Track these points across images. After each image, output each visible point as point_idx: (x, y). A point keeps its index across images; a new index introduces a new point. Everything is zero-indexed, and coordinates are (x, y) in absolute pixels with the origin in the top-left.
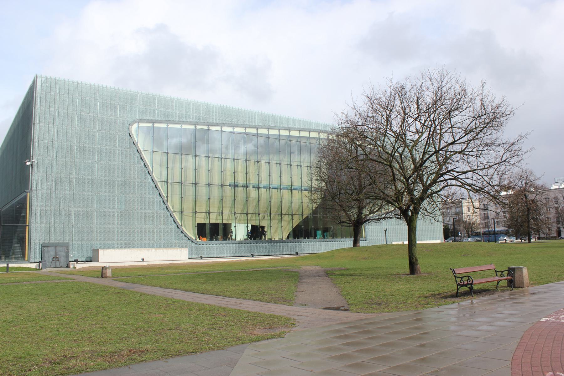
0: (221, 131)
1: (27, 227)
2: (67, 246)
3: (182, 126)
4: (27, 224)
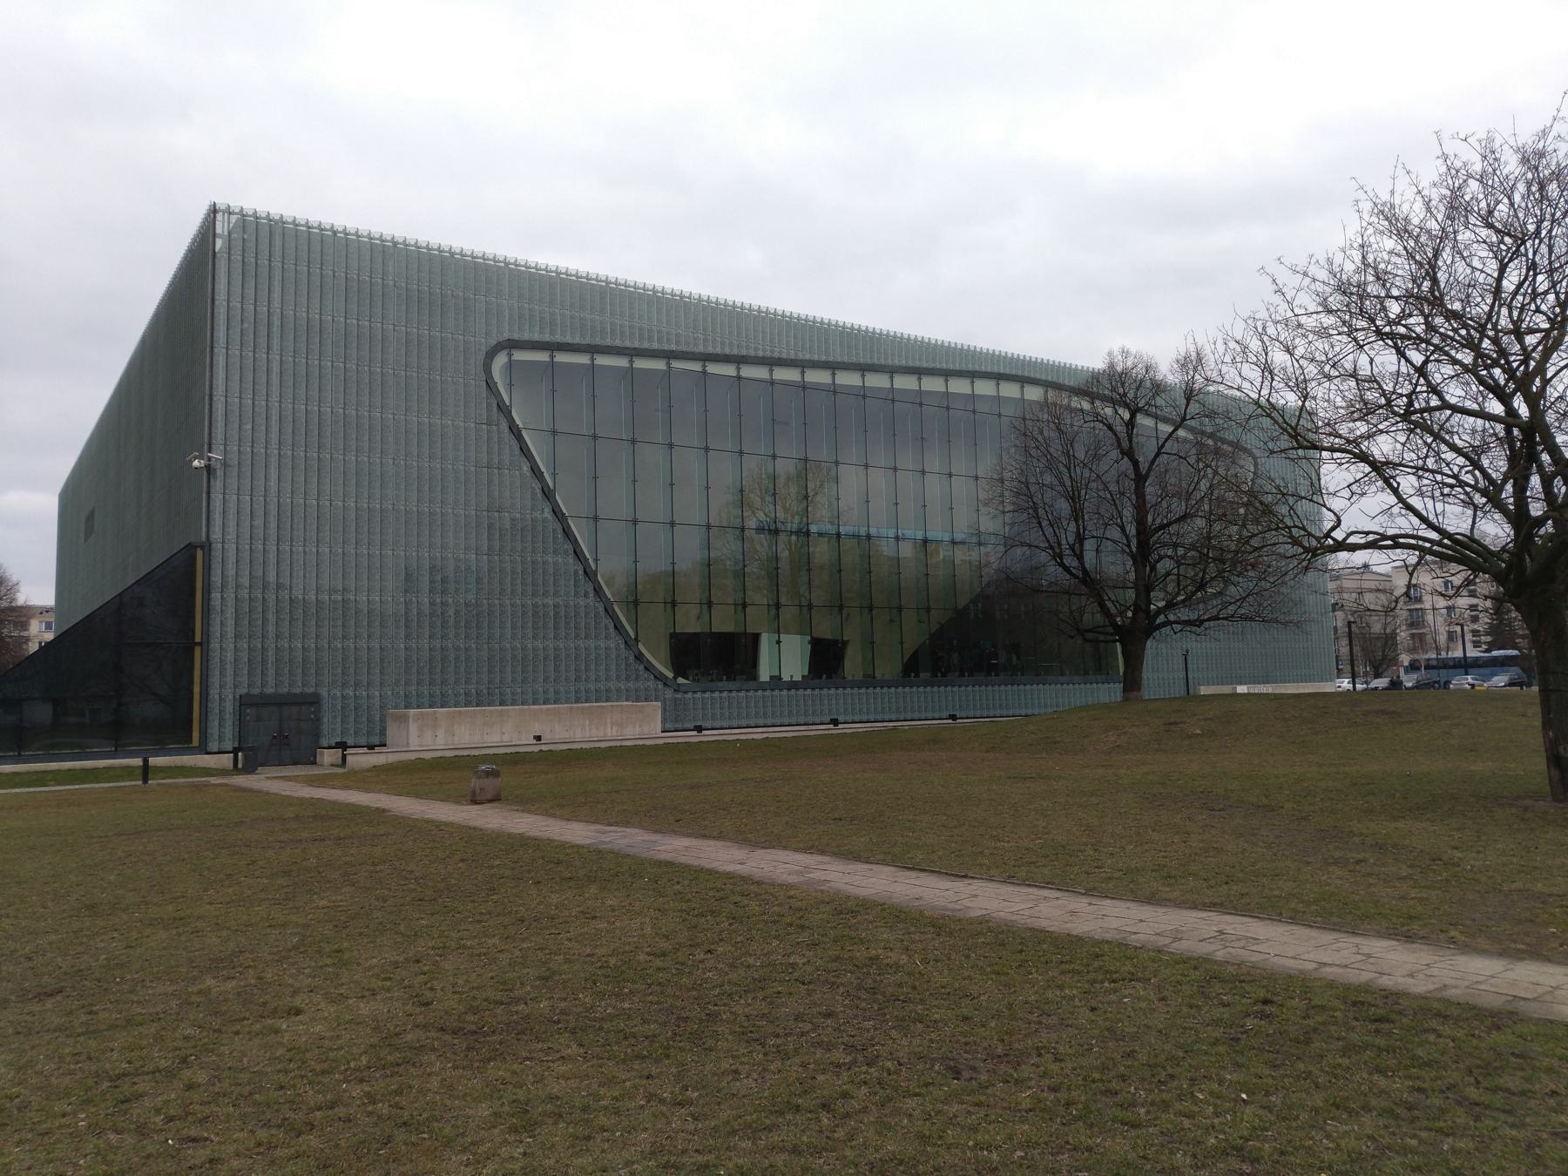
0: (704, 372)
1: (198, 650)
2: (313, 701)
3: (631, 362)
4: (198, 639)
